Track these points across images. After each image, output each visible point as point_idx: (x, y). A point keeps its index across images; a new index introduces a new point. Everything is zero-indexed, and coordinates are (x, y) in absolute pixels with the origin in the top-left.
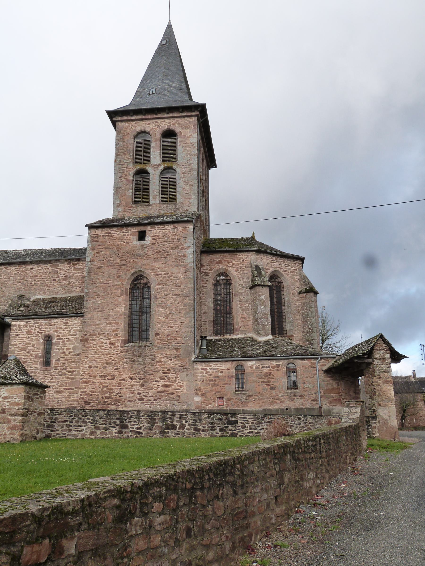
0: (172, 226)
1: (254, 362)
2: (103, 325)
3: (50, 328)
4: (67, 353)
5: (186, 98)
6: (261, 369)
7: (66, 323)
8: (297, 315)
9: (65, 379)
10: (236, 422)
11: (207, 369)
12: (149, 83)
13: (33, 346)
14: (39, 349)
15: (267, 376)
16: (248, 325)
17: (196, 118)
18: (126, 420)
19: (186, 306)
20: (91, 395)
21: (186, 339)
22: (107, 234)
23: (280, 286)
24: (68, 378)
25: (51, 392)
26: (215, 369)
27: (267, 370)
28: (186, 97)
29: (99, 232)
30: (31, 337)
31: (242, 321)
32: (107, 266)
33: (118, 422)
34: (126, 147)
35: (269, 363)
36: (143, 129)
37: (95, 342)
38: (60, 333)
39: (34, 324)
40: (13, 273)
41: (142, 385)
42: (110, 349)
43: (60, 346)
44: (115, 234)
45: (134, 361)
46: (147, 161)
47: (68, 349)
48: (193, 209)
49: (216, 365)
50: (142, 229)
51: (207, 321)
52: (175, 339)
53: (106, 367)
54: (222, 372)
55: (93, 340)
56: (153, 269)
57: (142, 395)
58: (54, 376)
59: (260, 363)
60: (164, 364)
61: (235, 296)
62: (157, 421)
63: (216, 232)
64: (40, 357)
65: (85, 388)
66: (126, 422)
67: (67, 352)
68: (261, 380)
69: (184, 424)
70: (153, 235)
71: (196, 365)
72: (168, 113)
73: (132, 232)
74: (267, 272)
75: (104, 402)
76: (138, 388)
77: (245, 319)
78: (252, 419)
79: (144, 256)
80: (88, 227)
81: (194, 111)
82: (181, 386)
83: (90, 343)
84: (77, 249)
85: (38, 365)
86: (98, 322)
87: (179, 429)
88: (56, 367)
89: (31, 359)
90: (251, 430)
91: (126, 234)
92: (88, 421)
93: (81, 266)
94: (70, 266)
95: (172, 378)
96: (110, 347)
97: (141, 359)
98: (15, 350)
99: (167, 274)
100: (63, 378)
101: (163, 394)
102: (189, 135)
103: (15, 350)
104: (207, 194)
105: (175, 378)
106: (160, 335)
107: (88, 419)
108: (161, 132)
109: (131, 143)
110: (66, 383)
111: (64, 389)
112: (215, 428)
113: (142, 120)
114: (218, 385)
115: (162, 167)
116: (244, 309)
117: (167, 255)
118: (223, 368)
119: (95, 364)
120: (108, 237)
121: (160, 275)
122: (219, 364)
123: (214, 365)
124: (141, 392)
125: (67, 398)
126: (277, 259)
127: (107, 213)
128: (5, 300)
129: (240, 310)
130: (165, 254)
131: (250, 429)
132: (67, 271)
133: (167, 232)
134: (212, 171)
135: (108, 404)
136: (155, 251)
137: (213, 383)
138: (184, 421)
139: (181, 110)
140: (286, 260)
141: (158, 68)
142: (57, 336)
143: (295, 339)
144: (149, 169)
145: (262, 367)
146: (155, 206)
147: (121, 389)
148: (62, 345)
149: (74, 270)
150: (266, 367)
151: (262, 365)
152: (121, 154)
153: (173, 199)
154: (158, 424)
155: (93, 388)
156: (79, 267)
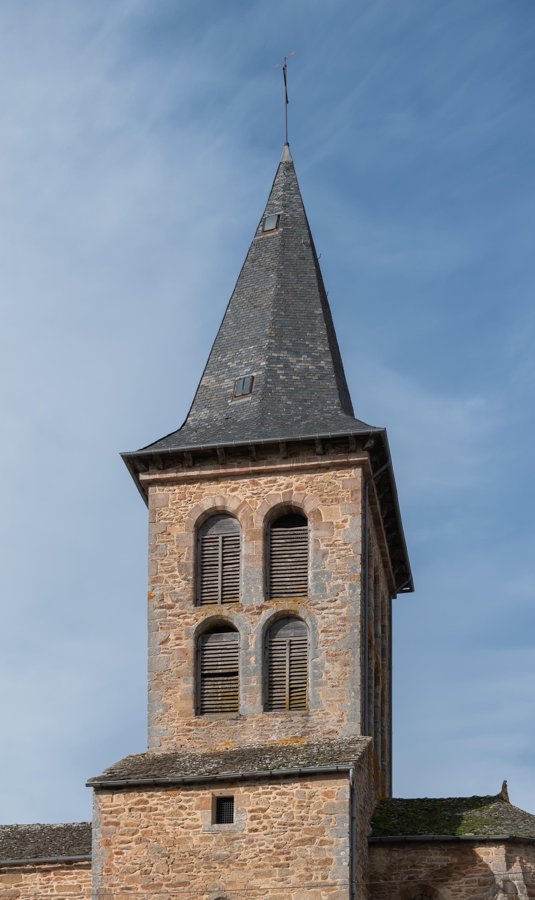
5: (333, 404)
12: (232, 360)
17: (359, 471)
22: (141, 806)
28: (332, 404)
29: (119, 799)
32: (144, 887)
34: (177, 556)
36: (219, 503)
44: (158, 806)
46: (230, 596)
63: (407, 785)
70: (251, 808)
72: (285, 459)
73: (202, 799)
79: (231, 862)
80: (92, 789)
81: (354, 451)
84: (59, 829)
93: (76, 878)
94: (49, 880)
102: (340, 521)
104: (386, 671)
108: (265, 511)
109: (183, 535)
113: (216, 478)
115: (266, 614)
117: (287, 859)
120: (143, 814)
127: (137, 744)
130: (282, 857)
132: (41, 891)
133: (286, 801)
134: (401, 603)
136: (257, 849)
141: (255, 311)
144: (237, 618)
146: (254, 728)
149: (59, 888)
152: (165, 575)
153: (297, 702)
156: (69, 882)
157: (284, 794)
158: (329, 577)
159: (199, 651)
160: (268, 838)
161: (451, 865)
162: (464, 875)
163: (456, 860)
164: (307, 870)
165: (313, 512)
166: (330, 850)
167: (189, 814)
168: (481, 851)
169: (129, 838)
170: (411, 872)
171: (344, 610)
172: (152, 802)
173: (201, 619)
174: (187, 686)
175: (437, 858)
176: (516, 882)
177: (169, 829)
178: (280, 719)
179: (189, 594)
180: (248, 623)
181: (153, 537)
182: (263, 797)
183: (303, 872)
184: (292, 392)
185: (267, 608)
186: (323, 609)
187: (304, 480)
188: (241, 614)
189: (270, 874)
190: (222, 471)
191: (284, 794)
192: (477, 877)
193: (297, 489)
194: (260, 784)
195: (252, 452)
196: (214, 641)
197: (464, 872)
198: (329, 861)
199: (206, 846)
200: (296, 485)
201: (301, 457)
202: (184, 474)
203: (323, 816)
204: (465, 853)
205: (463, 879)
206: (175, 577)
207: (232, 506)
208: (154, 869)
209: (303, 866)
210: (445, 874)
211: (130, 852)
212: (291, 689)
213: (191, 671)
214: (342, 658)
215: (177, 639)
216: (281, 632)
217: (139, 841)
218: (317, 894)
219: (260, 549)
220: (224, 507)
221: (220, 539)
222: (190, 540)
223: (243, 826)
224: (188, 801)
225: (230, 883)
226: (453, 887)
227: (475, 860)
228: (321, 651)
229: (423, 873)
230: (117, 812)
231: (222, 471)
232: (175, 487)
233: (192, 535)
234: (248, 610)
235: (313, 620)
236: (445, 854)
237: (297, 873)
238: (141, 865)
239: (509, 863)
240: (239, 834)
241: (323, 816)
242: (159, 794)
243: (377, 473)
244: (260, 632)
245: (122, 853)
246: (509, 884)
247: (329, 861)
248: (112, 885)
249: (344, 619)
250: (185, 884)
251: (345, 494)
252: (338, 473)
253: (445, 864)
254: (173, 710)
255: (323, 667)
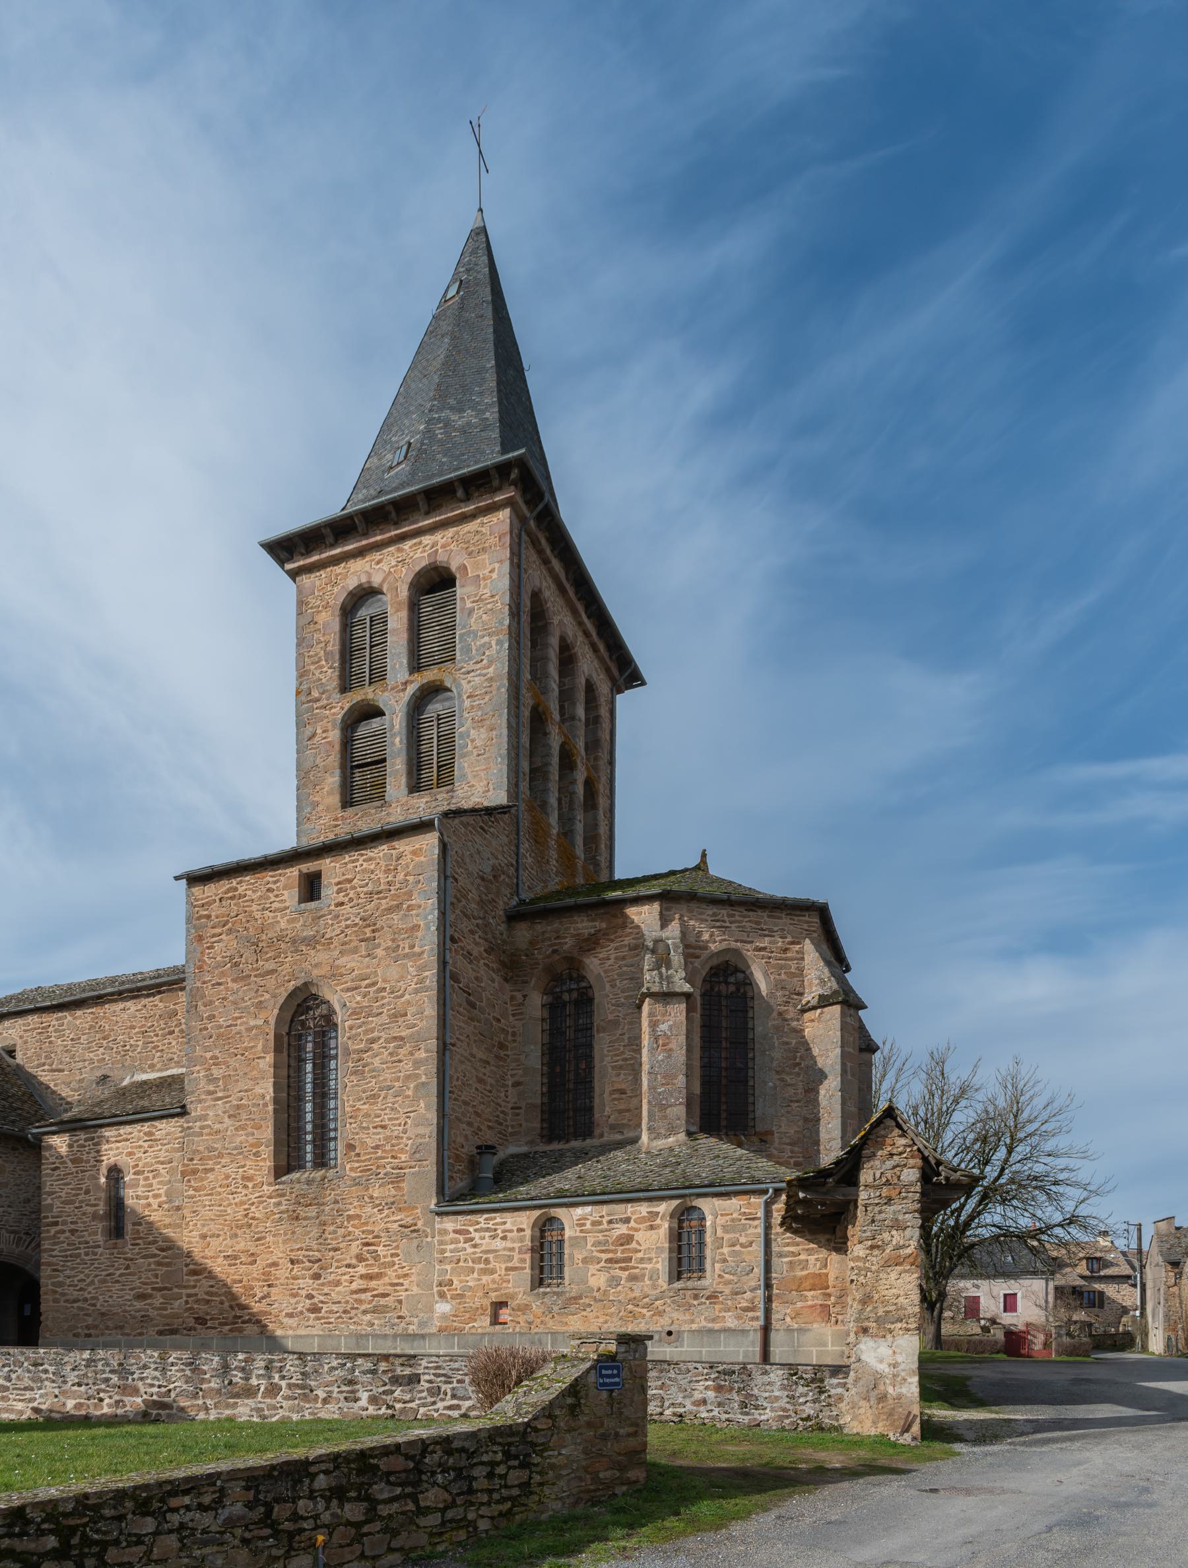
0: (385, 847)
1: (588, 1209)
2: (229, 1133)
3: (118, 1148)
4: (155, 1207)
6: (605, 1226)
7: (150, 1134)
8: (788, 1074)
9: (153, 1266)
10: (414, 1379)
11: (469, 1232)
13: (87, 1192)
14: (99, 1199)
15: (622, 1245)
16: (629, 1110)
18: (133, 1373)
19: (418, 1068)
20: (208, 1302)
21: (417, 1156)
23: (745, 993)
24: (159, 1264)
25: (128, 1297)
26: (488, 1230)
27: (622, 1229)
29: (211, 890)
30: (82, 1171)
31: (614, 1099)
32: (234, 981)
33: (115, 1379)
35: (630, 1208)
36: (364, 580)
37: (211, 1176)
38: (140, 1159)
39: (86, 1140)
40: (87, 1026)
41: (317, 1276)
42: (244, 1192)
43: (140, 1189)
45: (297, 1218)
46: (378, 676)
47: (156, 1196)
48: (357, 773)
49: (491, 1219)
50: (308, 867)
51: (523, 1104)
52: (393, 1157)
53: (236, 1235)
54: (504, 1238)
55: (207, 1171)
56: (335, 974)
57: (316, 1300)
58: (132, 1260)
59: (605, 1209)
60: (366, 1224)
61: (598, 1032)
62: (207, 1376)
64: (101, 1218)
65: (195, 1287)
66: (133, 1380)
67: (155, 1203)
68: (604, 1256)
69: (276, 1384)
70: (337, 880)
71: (441, 1223)
72: (427, 514)
74: (698, 957)
75: (236, 1317)
76: (306, 1284)
77: (623, 1092)
78: (458, 1370)
79: (318, 942)
81: (499, 489)
82: (406, 1275)
83: (202, 1179)
85: (99, 1237)
86: (217, 1126)
87: (263, 1397)
88: (135, 1239)
89: (85, 1222)
90: (455, 1402)
91: (274, 887)
92: (44, 1376)
95: (385, 1257)
96: (246, 1187)
97: (312, 1211)
98: (52, 1205)
99: (374, 984)
100: (149, 1264)
101: (363, 1296)
102: (486, 572)
103: (52, 1205)
105: (392, 1255)
106: (357, 1151)
107: (46, 1371)
109: (329, 620)
110: (156, 1276)
111: (153, 1289)
112: (358, 1395)
113: (361, 553)
114: (493, 1271)
115: (411, 689)
116: (621, 1067)
117: (373, 931)
118: (508, 1226)
119: (213, 1228)
121: (356, 988)
122: (499, 1218)
123: (486, 1219)
124: (314, 1293)
125: (160, 1309)
126: (733, 916)
128: (75, 1091)
129: (610, 1069)
130: (368, 930)
131: (454, 1396)
135: (243, 1322)
136: (343, 924)
137: (482, 1266)
138: (277, 1376)
139: (460, 493)
140: (763, 916)
142: (134, 1167)
143: (777, 1140)
145: (610, 1222)
147: (269, 1286)
148: (144, 1186)
150: (621, 1220)
151: (608, 1215)
152: (312, 667)
154: (212, 1385)
155: (212, 1286)
157: (370, 859)
158: (476, 636)
159: (347, 743)
160: (354, 910)
161: (599, 931)
162: (612, 941)
163: (604, 925)
164: (393, 940)
165: (459, 568)
166: (417, 916)
167: (277, 896)
168: (632, 912)
169: (219, 930)
170: (555, 944)
171: (491, 670)
172: (241, 890)
173: (347, 706)
174: (333, 780)
175: (584, 925)
176: (670, 942)
177: (258, 915)
178: (424, 800)
179: (335, 683)
180: (393, 702)
181: (300, 629)
182: (350, 866)
183: (390, 943)
184: (449, 449)
185: (412, 682)
186: (468, 673)
187: (450, 535)
188: (386, 694)
189: (355, 951)
190: (364, 542)
191: (370, 859)
192: (627, 941)
193: (443, 546)
194: (347, 853)
195: (390, 513)
196: (364, 729)
197: (612, 937)
198: (416, 927)
199: (293, 929)
200: (441, 542)
201: (444, 509)
202: (327, 554)
203: (411, 878)
204: (615, 916)
205: (612, 945)
206: (322, 667)
207: (376, 581)
208: (243, 960)
209: (389, 936)
210: (591, 943)
211: (220, 944)
212: (439, 767)
213: (337, 764)
214: (488, 722)
215: (324, 732)
216: (430, 707)
217: (230, 931)
218: (404, 966)
219: (405, 620)
220: (369, 582)
221: (368, 621)
222: (336, 625)
223: (329, 901)
224: (275, 882)
225: (316, 965)
226: (601, 956)
227: (626, 922)
228: (467, 719)
229: (569, 943)
230: (209, 904)
231: (364, 542)
232: (322, 572)
233: (337, 619)
234: (392, 689)
235: (459, 686)
236: (593, 920)
237: (384, 945)
238: (231, 957)
239: (664, 922)
240: (325, 911)
241: (411, 878)
242: (247, 878)
243: (535, 513)
244: (405, 710)
245: (213, 947)
246: (661, 944)
247: (416, 927)
248: (204, 983)
249: (491, 679)
250: (273, 972)
251: (493, 540)
252: (485, 519)
253: (592, 931)
254: (320, 807)
255: (468, 736)
